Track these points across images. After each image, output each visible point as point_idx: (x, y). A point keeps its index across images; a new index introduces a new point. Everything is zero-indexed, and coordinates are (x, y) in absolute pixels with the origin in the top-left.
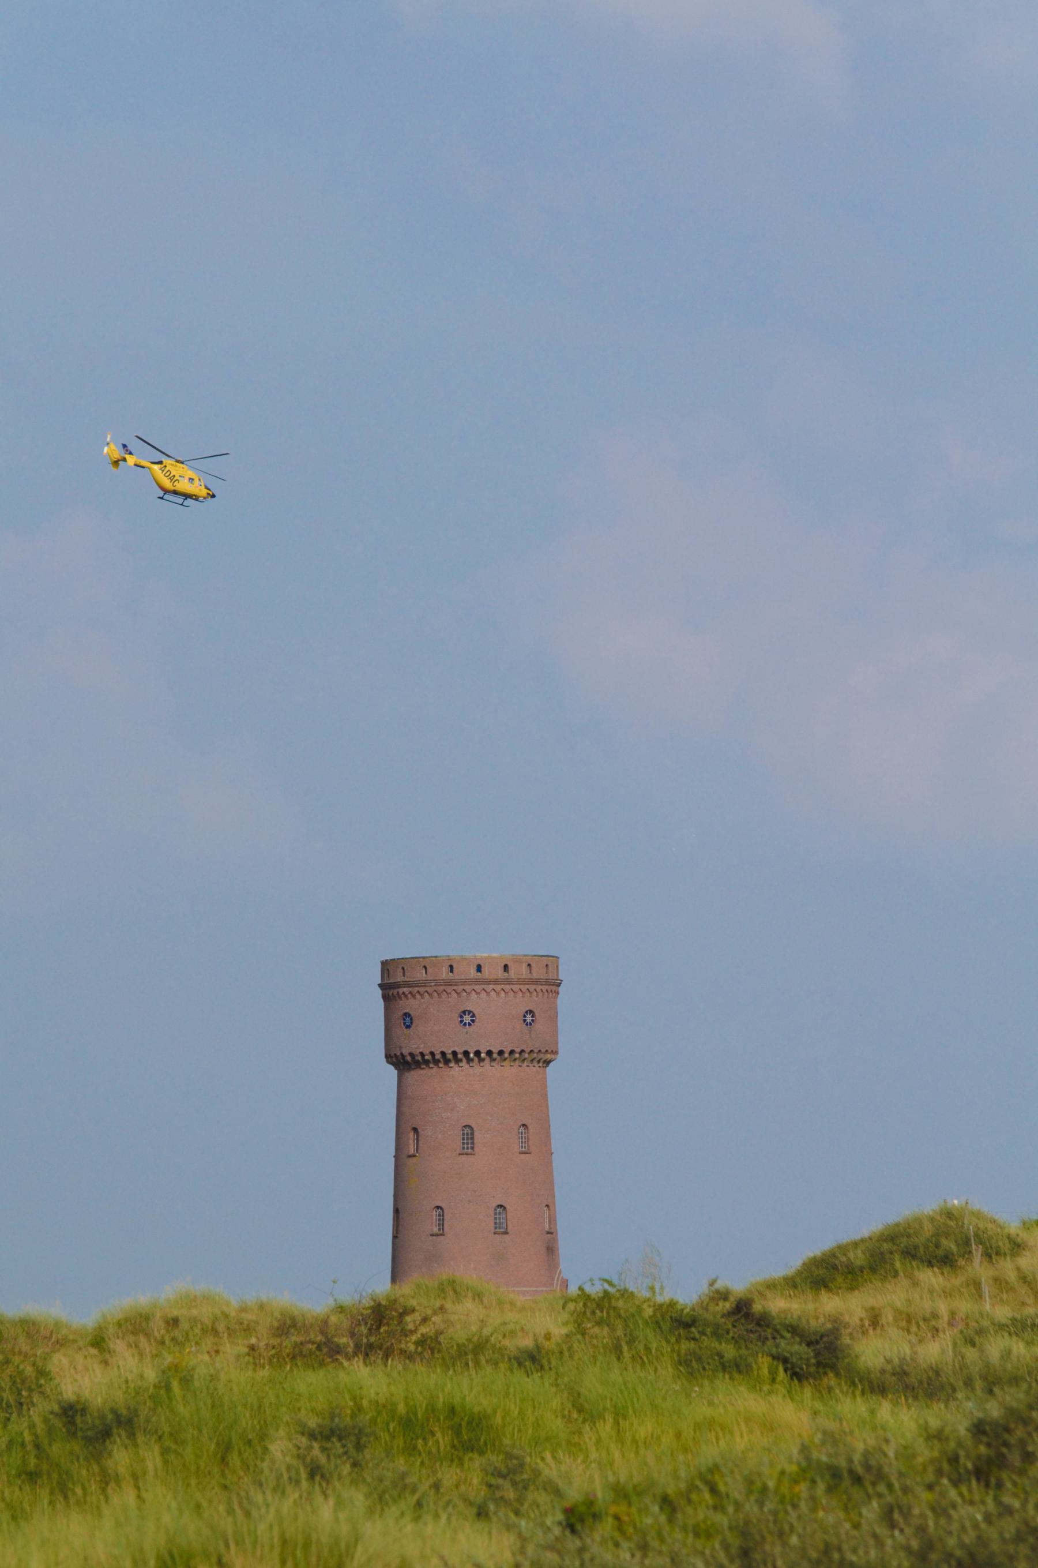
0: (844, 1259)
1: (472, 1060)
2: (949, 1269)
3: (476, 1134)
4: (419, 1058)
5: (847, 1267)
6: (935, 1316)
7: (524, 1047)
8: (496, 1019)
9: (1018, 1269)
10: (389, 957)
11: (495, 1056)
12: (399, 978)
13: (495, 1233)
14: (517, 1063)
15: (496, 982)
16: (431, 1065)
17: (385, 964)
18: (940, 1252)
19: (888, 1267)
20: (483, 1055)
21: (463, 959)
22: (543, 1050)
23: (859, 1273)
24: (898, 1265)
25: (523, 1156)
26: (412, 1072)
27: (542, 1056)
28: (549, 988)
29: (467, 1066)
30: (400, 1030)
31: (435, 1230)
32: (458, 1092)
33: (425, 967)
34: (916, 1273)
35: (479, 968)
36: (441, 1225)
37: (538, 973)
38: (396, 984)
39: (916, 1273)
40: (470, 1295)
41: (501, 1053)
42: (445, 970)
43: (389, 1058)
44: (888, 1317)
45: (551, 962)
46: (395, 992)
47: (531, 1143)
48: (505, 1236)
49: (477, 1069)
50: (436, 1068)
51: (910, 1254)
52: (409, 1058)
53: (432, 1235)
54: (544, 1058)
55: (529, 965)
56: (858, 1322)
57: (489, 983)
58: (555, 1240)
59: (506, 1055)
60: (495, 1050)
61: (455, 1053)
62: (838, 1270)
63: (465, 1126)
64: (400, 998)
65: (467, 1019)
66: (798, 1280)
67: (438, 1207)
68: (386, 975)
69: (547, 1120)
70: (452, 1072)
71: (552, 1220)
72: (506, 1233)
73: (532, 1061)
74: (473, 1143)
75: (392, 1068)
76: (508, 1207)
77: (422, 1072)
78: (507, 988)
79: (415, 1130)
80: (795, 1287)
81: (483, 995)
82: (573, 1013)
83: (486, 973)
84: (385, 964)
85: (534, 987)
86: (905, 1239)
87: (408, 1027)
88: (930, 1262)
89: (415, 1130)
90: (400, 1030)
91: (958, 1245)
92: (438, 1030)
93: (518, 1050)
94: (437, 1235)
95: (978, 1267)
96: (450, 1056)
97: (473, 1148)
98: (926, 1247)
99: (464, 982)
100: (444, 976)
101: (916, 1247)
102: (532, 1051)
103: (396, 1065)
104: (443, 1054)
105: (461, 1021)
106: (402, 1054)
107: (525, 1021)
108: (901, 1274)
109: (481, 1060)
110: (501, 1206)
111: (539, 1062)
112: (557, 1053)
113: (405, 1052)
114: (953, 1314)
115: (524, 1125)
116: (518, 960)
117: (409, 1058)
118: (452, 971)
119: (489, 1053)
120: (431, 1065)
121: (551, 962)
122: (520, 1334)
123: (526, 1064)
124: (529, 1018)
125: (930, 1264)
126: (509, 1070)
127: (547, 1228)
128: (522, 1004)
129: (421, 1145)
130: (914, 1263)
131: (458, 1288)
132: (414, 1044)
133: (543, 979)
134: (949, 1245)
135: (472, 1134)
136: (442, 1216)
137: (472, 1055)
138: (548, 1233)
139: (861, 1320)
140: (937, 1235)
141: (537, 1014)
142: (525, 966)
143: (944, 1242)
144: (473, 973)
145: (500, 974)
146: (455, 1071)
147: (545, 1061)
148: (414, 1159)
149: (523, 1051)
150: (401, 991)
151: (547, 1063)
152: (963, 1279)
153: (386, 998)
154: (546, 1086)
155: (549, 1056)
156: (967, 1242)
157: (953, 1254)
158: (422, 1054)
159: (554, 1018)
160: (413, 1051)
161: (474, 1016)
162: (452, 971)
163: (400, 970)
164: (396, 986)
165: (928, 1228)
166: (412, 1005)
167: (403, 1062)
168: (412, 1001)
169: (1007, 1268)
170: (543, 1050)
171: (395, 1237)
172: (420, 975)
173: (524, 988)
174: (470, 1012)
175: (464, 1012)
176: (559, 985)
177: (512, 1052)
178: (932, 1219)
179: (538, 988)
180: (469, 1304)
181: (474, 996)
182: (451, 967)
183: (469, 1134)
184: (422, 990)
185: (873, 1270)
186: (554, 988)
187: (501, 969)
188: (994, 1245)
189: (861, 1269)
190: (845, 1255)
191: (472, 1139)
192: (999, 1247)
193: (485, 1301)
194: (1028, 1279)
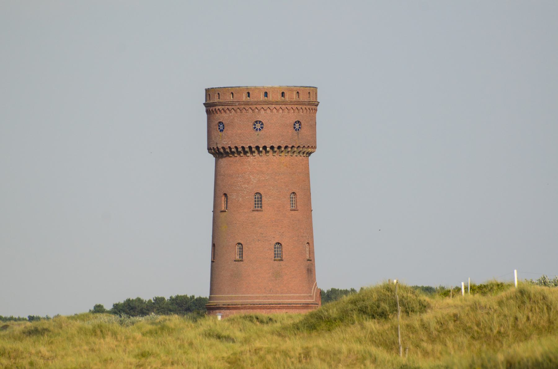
0: (326, 313)
1: (261, 152)
2: (384, 320)
3: (263, 198)
4: (228, 150)
5: (328, 318)
6: (340, 352)
7: (294, 144)
8: (276, 126)
9: (422, 320)
10: (210, 87)
11: (276, 149)
12: (216, 100)
13: (274, 260)
14: (290, 154)
15: (277, 103)
16: (236, 155)
17: (207, 91)
18: (380, 310)
19: (350, 318)
20: (268, 149)
21: (256, 88)
22: (306, 146)
23: (333, 321)
24: (355, 317)
25: (293, 212)
26: (224, 159)
27: (305, 150)
28: (310, 107)
29: (258, 156)
30: (216, 133)
31: (237, 257)
32: (253, 171)
33: (232, 93)
34: (365, 322)
35: (266, 94)
36: (241, 254)
37: (303, 98)
38: (215, 104)
39: (365, 322)
40: (110, 333)
41: (279, 147)
42: (244, 95)
43: (209, 149)
44: (314, 353)
45: (312, 91)
46: (214, 108)
47: (298, 204)
48: (281, 262)
49: (264, 158)
50: (238, 156)
51: (363, 311)
52: (222, 150)
53: (235, 261)
54: (307, 150)
55: (298, 92)
56: (297, 355)
57: (272, 103)
58: (313, 265)
59: (283, 149)
60: (276, 146)
61: (250, 148)
62: (323, 320)
63: (257, 193)
64: (216, 112)
65: (258, 126)
66: (299, 325)
67: (239, 244)
68: (208, 98)
69: (309, 190)
70: (249, 159)
71: (312, 252)
72: (282, 260)
73: (299, 152)
74: (261, 204)
75: (212, 156)
76: (283, 244)
77: (230, 159)
78: (283, 107)
79: (225, 195)
80: (298, 329)
81: (268, 111)
82: (327, 124)
83: (270, 97)
84: (207, 91)
85: (301, 106)
86: (362, 302)
87: (221, 131)
88: (373, 316)
89: (225, 195)
90: (216, 133)
91: (390, 307)
92: (239, 133)
93: (290, 146)
94: (238, 261)
95: (400, 319)
96: (247, 150)
97: (261, 207)
98: (372, 307)
99: (257, 103)
100: (244, 99)
101: (366, 307)
102: (299, 147)
103: (214, 154)
104: (243, 148)
105: (255, 128)
106: (217, 148)
107: (295, 128)
108: (357, 322)
109: (267, 152)
110: (279, 243)
111: (304, 153)
112: (315, 148)
113: (220, 146)
114: (350, 351)
115: (293, 193)
116: (290, 89)
117: (222, 150)
118: (249, 96)
119: (272, 148)
120: (236, 155)
121: (312, 91)
122: (109, 361)
123: (295, 154)
124: (297, 126)
125: (373, 317)
126: (284, 158)
127: (308, 258)
128: (292, 117)
129: (228, 204)
130: (364, 316)
131: (104, 330)
132: (225, 141)
133: (306, 101)
134: (385, 306)
135: (261, 198)
136: (241, 249)
137: (261, 149)
138: (308, 260)
139: (300, 354)
140: (378, 300)
141: (302, 123)
142: (295, 93)
143: (383, 305)
144: (262, 97)
145: (279, 98)
146: (252, 159)
147: (307, 153)
148: (225, 214)
149: (293, 147)
150: (217, 108)
151: (309, 154)
152: (407, 322)
153: (208, 112)
154: (308, 168)
155: (310, 150)
156: (396, 305)
157: (386, 311)
158: (230, 148)
159: (313, 126)
160: (224, 146)
161: (262, 124)
162: (249, 96)
163: (217, 94)
164: (214, 105)
165: (375, 296)
166: (224, 117)
167: (218, 153)
168: (224, 114)
169: (415, 320)
170: (306, 146)
171: (212, 262)
172: (229, 98)
173: (294, 107)
174: (260, 122)
175: (256, 122)
176: (317, 105)
177: (286, 147)
178: (378, 292)
179: (304, 107)
180: (108, 339)
181: (262, 112)
182: (249, 93)
183: (259, 198)
184: (230, 107)
185: (342, 320)
186: (314, 107)
187: (280, 96)
188: (410, 307)
189: (335, 319)
190: (327, 311)
191: (261, 201)
192: (413, 307)
193: (119, 337)
194: (426, 326)
